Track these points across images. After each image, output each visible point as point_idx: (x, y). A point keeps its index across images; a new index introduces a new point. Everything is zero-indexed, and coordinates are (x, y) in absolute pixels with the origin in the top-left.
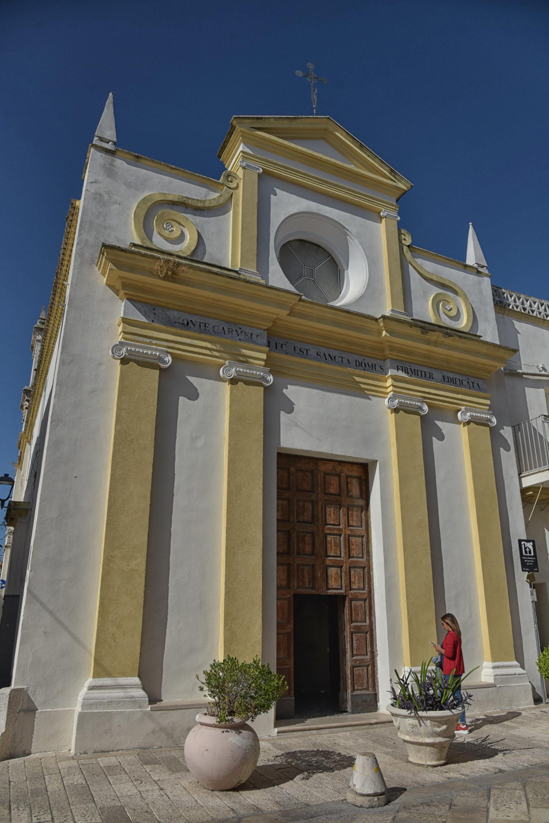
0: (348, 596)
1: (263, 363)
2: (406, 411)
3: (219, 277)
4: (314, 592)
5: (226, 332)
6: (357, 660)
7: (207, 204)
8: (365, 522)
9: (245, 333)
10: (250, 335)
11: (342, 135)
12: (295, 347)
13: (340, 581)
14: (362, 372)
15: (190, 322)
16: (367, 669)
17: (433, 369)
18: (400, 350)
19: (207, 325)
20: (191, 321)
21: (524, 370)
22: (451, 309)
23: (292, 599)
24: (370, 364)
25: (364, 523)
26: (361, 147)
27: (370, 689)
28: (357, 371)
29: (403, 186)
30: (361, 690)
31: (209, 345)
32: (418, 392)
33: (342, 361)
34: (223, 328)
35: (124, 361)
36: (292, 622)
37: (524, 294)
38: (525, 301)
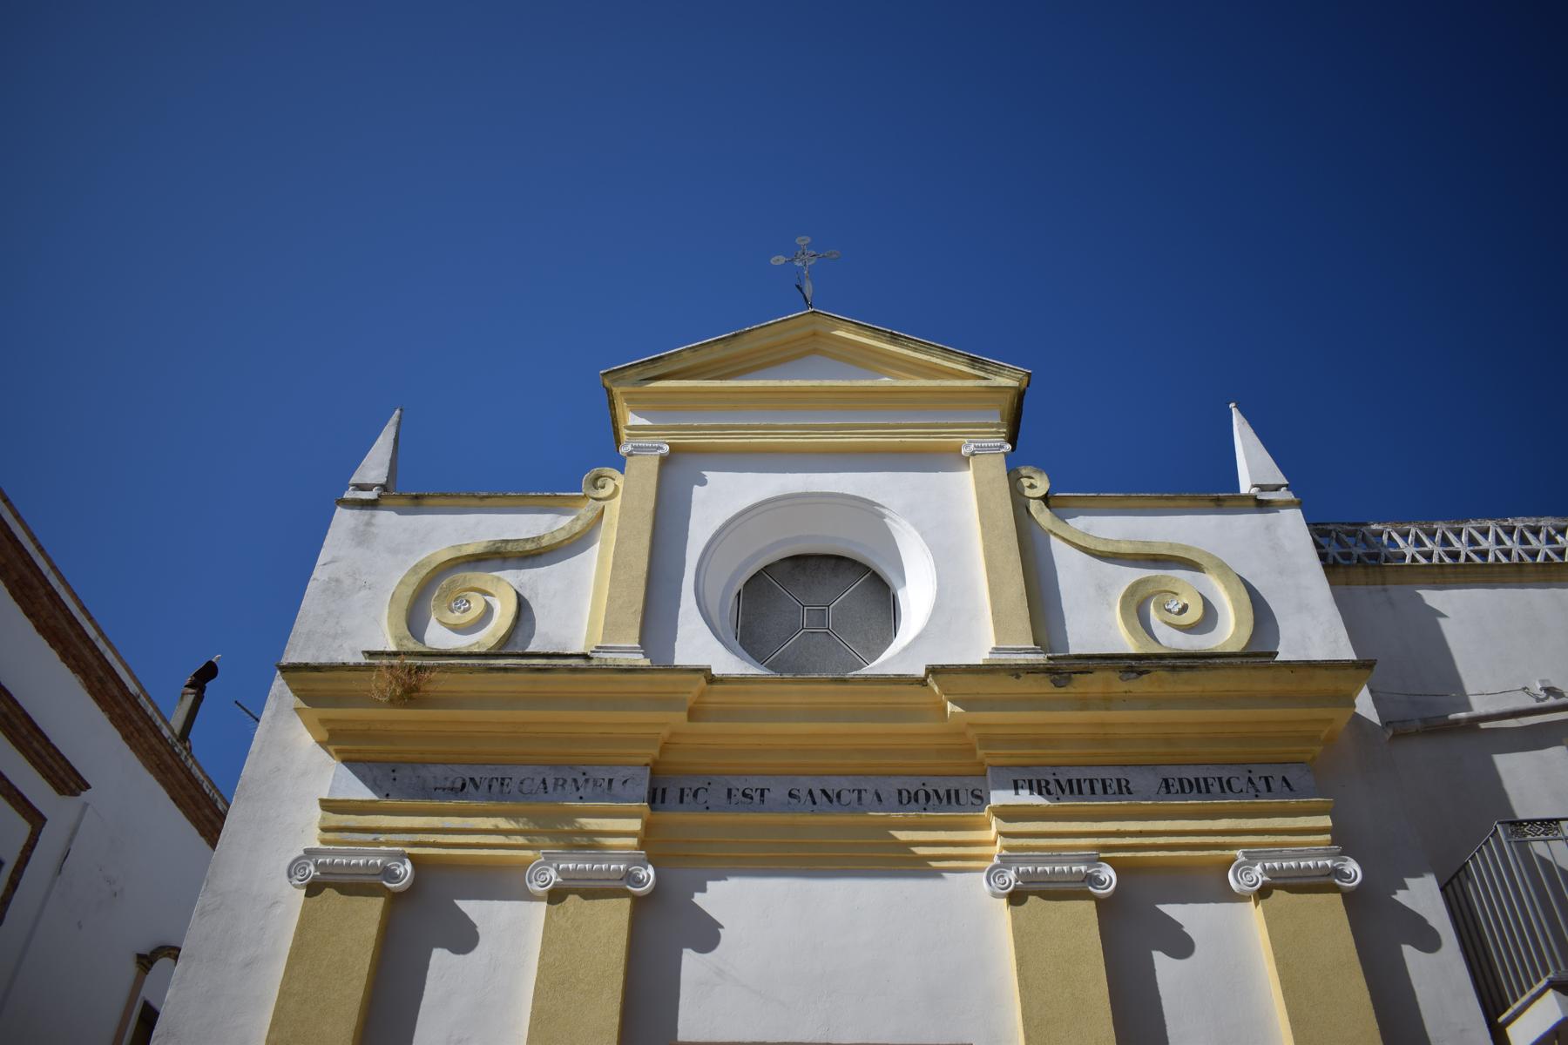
1: (633, 841)
3: (511, 675)
5: (550, 788)
7: (545, 543)
9: (595, 781)
11: (848, 331)
18: (1012, 741)
21: (1479, 707)
22: (1184, 609)
24: (942, 793)
26: (894, 339)
28: (897, 816)
29: (1007, 380)
31: (503, 823)
32: (1083, 839)
33: (860, 798)
34: (544, 782)
37: (1443, 520)
38: (1451, 537)
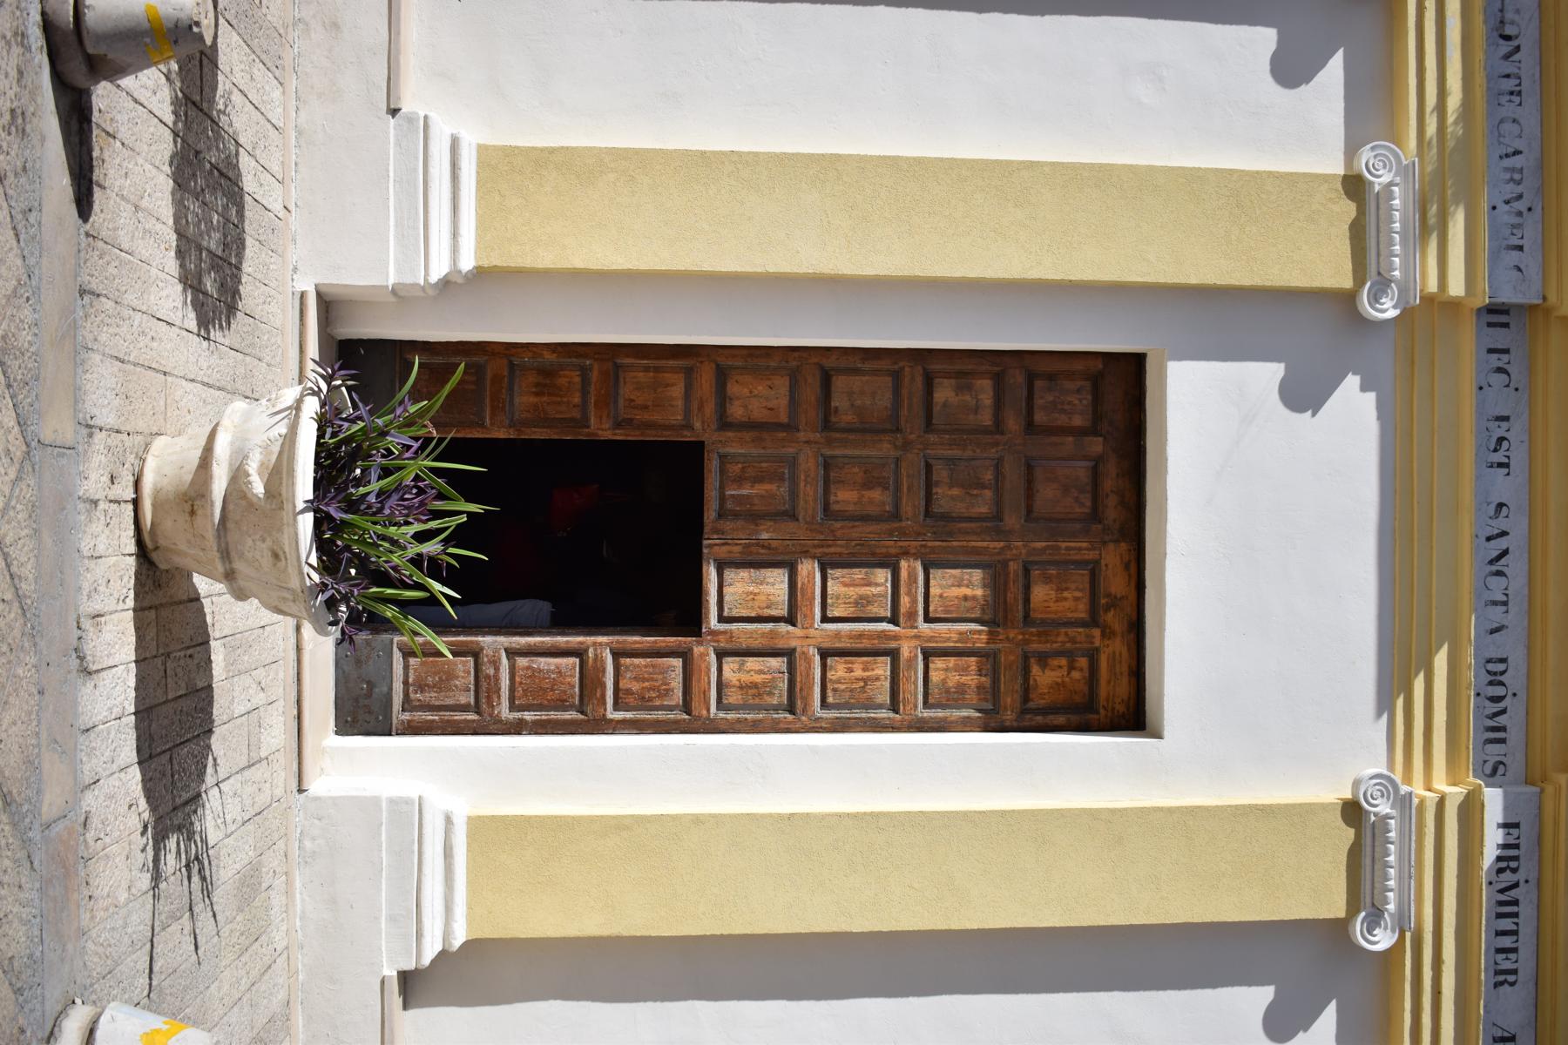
0: (700, 643)
1: (1432, 286)
2: (1355, 854)
4: (710, 514)
5: (1508, 162)
6: (497, 669)
8: (945, 719)
9: (1519, 226)
10: (1515, 241)
12: (1506, 419)
13: (745, 613)
14: (1470, 676)
15: (1515, 43)
16: (464, 708)
17: (1531, 986)
19: (1516, 99)
20: (1518, 49)
23: (688, 436)
24: (1502, 720)
25: (940, 713)
27: (406, 716)
28: (1469, 657)
30: (406, 683)
31: (1454, 101)
33: (1495, 603)
34: (1517, 152)
35: (1352, 811)
36: (619, 436)
